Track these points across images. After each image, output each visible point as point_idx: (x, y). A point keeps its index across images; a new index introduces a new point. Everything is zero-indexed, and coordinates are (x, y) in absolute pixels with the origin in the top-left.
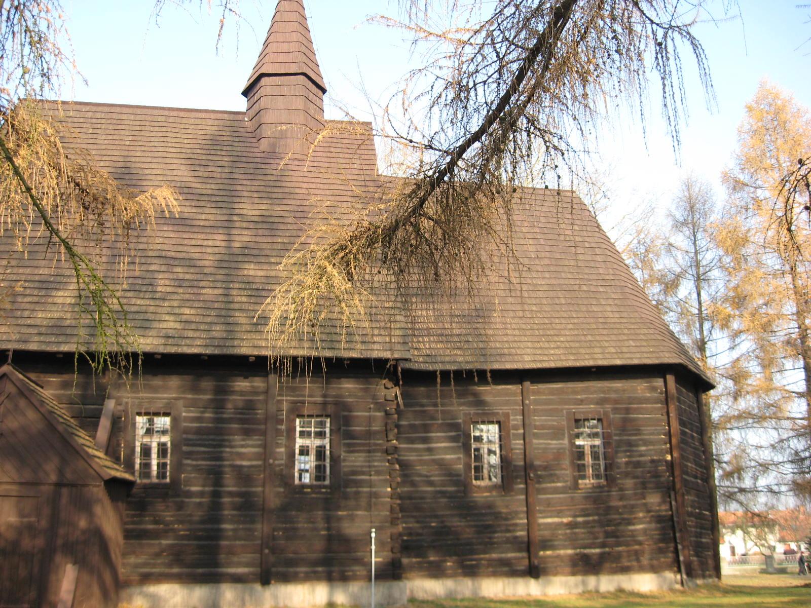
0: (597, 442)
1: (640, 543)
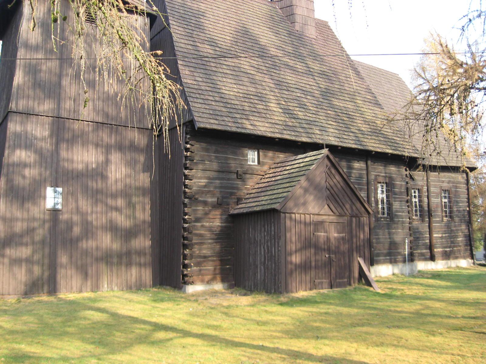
0: (446, 200)
1: (460, 246)
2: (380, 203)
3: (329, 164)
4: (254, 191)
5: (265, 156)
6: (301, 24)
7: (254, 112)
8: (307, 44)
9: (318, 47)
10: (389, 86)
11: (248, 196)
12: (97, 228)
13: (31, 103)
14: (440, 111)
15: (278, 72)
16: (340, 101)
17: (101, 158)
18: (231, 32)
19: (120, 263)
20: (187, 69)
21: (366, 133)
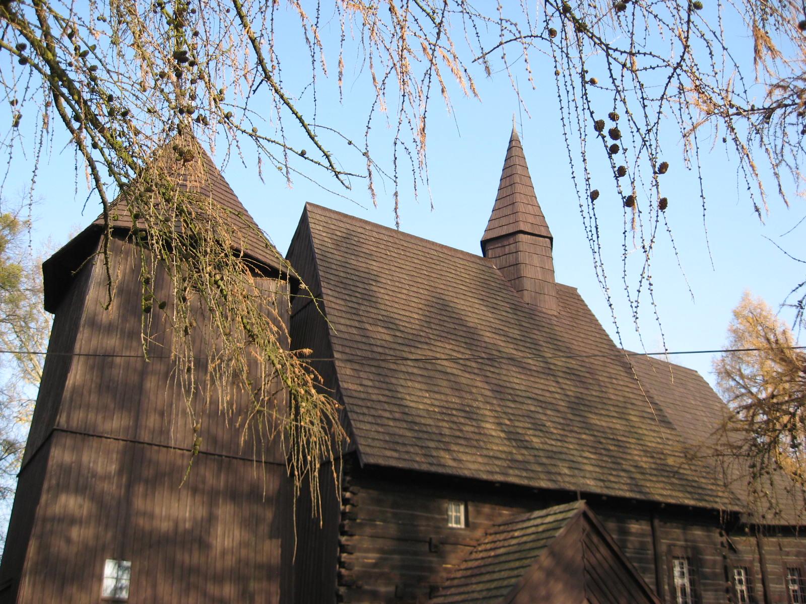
0: (796, 587)
2: (679, 594)
3: (588, 527)
4: (459, 574)
5: (479, 513)
6: (533, 294)
7: (459, 437)
8: (543, 324)
9: (562, 329)
10: (682, 390)
11: (448, 583)
13: (91, 416)
14: (775, 442)
15: (497, 371)
16: (603, 418)
17: (201, 512)
18: (420, 306)
20: (349, 365)
21: (648, 471)
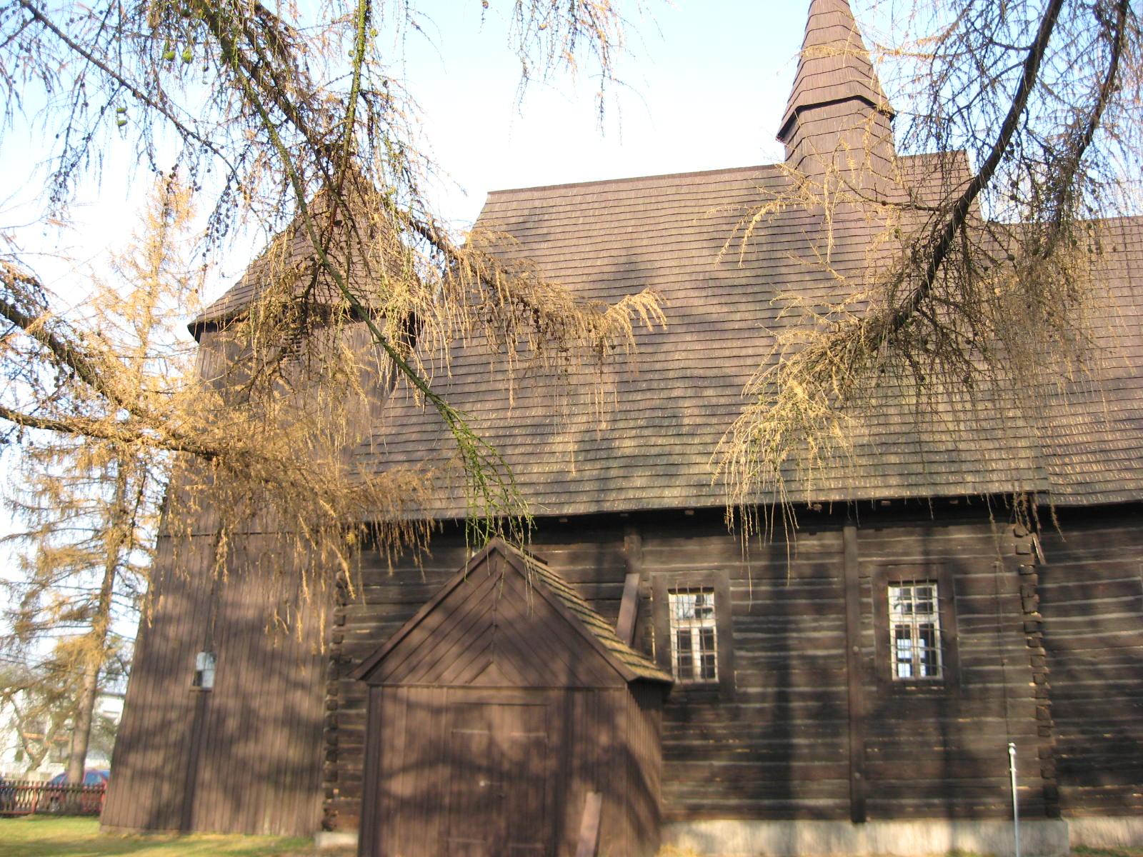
12: (265, 721)
19: (293, 788)
